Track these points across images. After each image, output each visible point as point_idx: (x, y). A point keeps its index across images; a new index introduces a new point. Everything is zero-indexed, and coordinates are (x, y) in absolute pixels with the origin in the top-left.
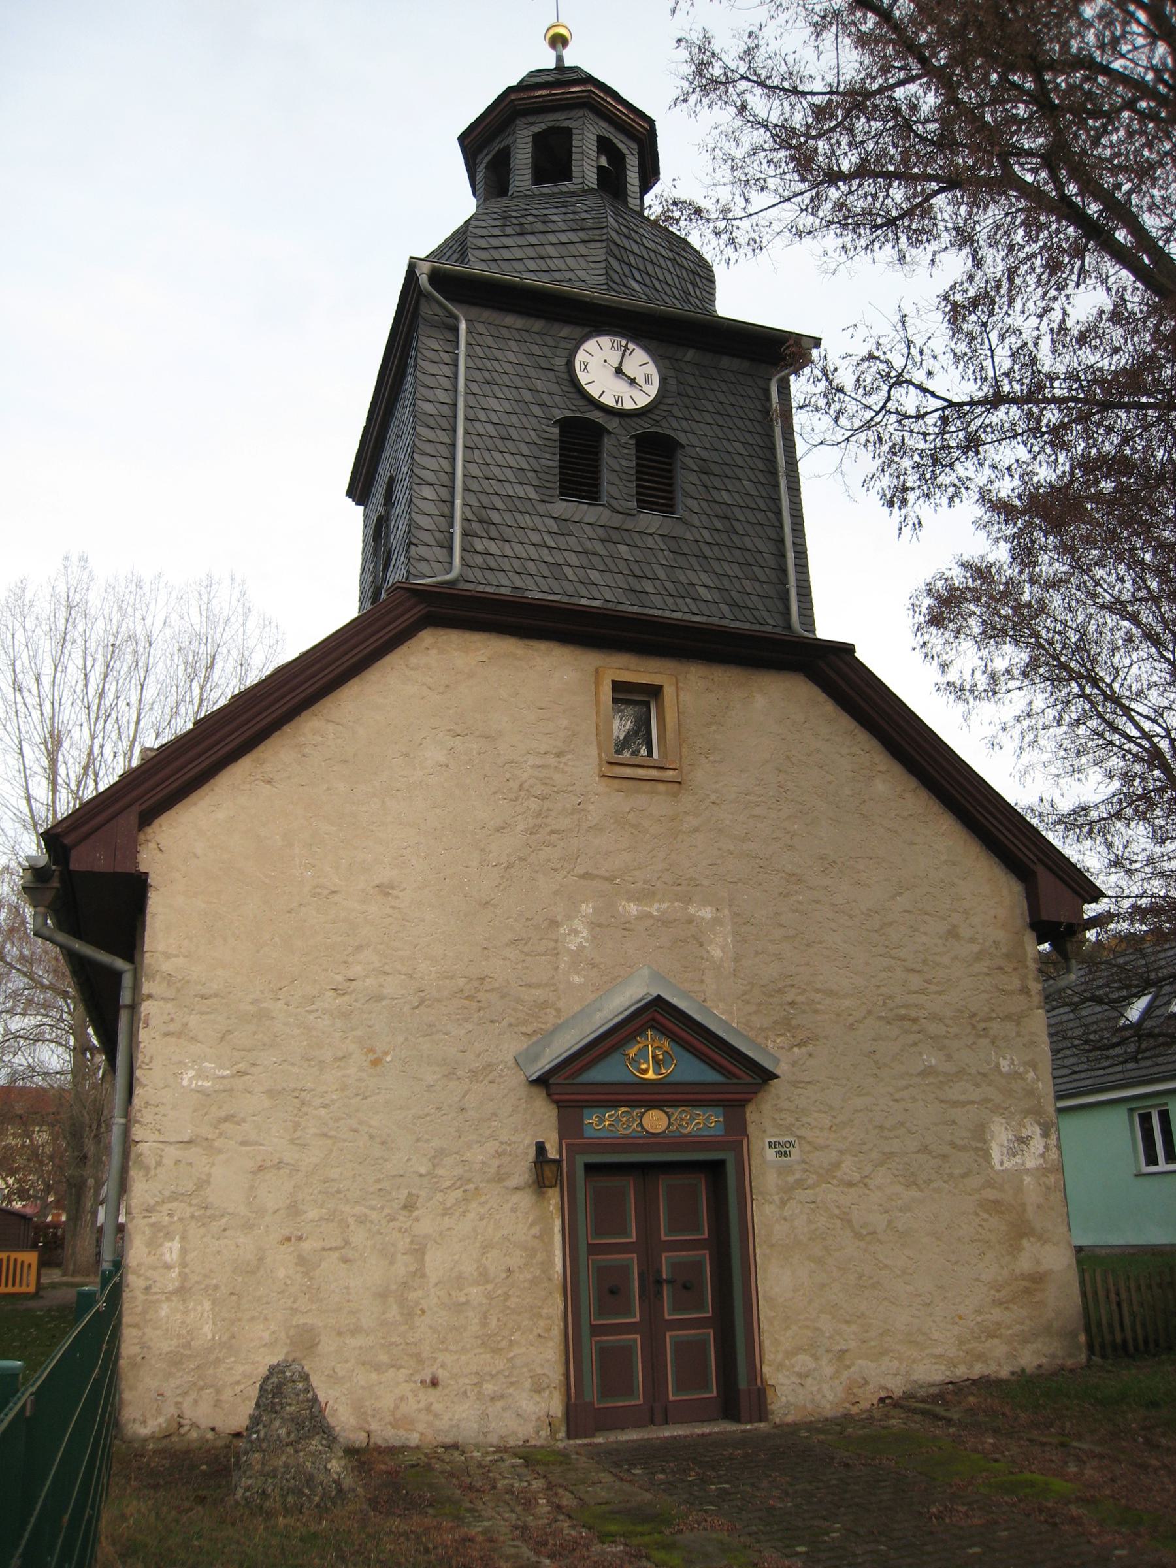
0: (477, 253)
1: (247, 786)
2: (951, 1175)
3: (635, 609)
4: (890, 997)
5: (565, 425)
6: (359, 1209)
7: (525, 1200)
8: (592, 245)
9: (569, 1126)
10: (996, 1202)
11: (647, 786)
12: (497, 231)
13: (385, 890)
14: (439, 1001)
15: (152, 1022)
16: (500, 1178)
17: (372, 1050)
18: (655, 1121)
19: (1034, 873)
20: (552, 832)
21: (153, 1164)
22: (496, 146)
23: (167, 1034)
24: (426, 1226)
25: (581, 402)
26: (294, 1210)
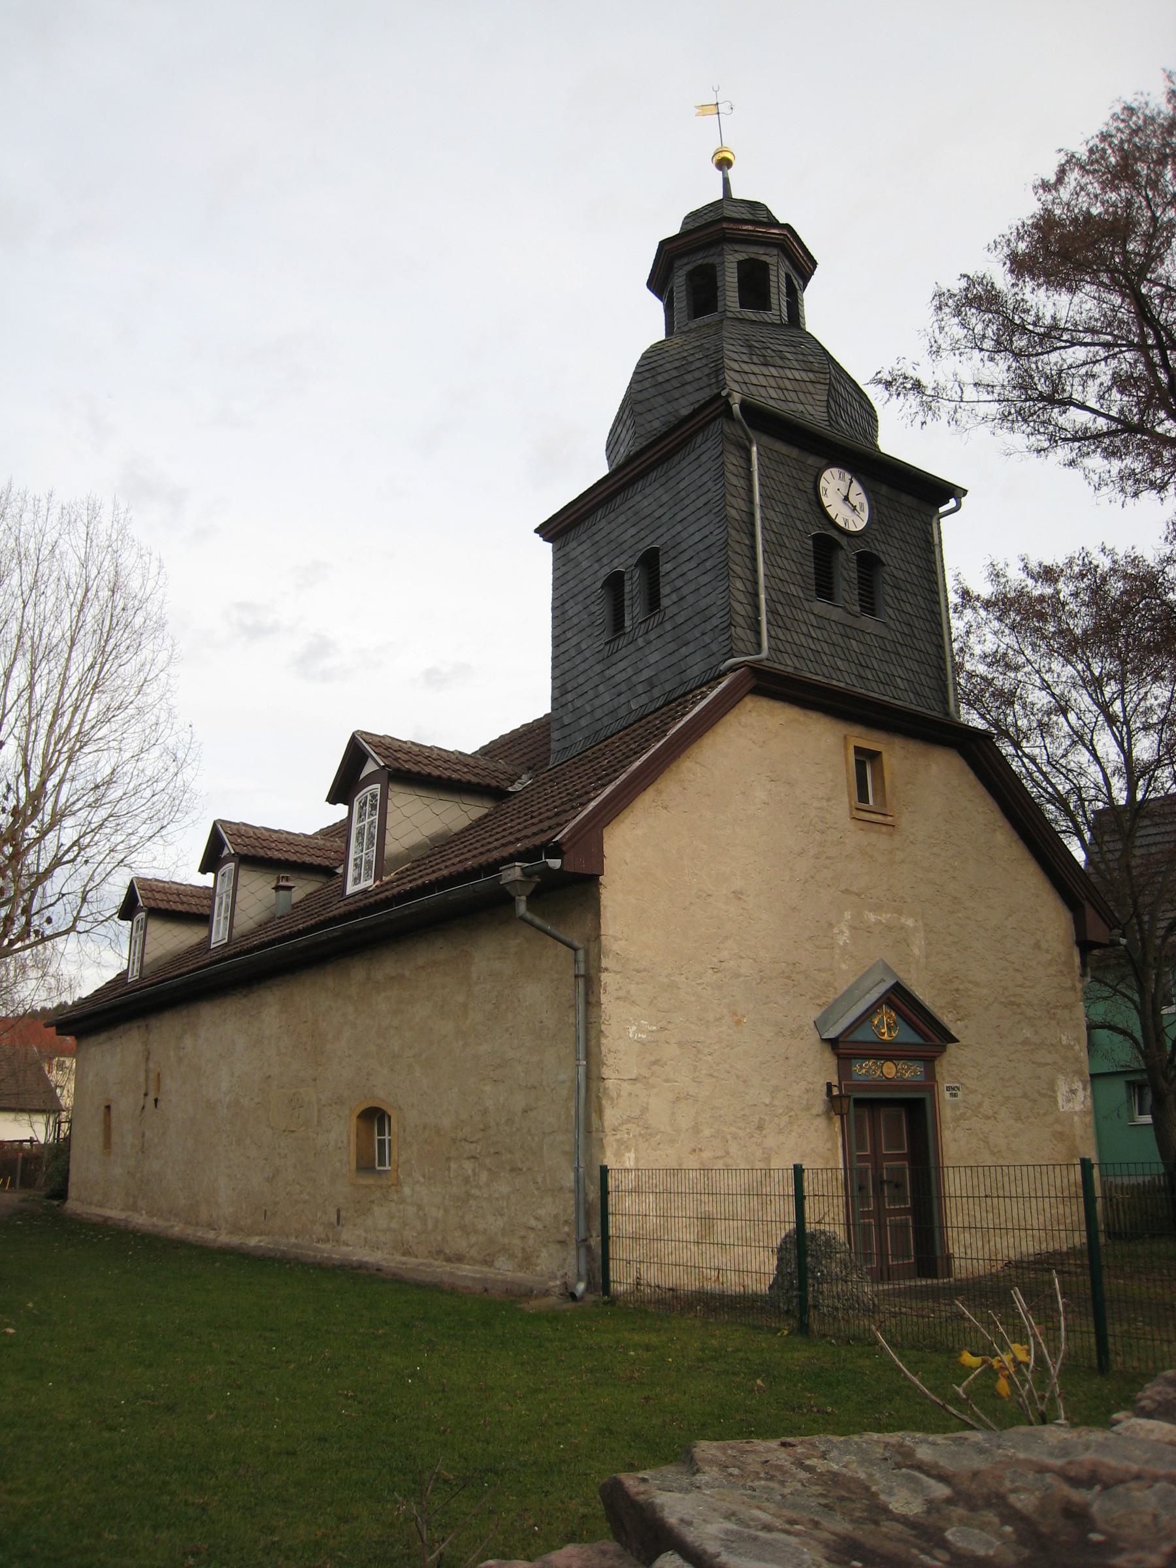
0: (732, 373)
1: (652, 810)
2: (1038, 1114)
3: (863, 691)
4: (1006, 989)
5: (816, 538)
6: (733, 1129)
7: (821, 1123)
8: (819, 386)
9: (844, 1071)
10: (1061, 1133)
11: (876, 827)
12: (745, 358)
13: (738, 895)
14: (771, 979)
15: (608, 989)
16: (808, 1108)
17: (735, 1014)
18: (890, 1070)
19: (1082, 906)
20: (828, 858)
21: (615, 1095)
22: (699, 260)
23: (618, 998)
24: (771, 1142)
25: (825, 521)
26: (696, 1130)
